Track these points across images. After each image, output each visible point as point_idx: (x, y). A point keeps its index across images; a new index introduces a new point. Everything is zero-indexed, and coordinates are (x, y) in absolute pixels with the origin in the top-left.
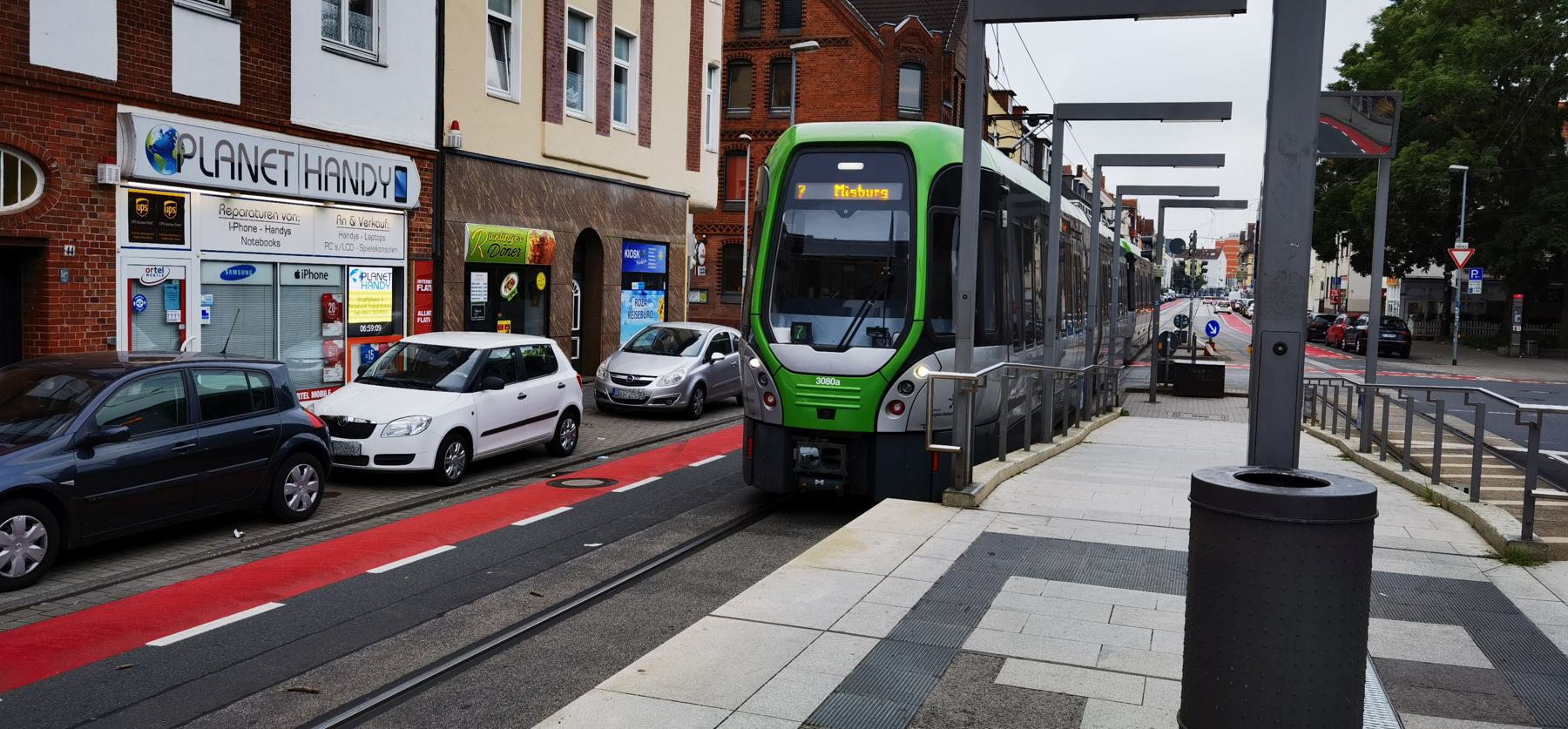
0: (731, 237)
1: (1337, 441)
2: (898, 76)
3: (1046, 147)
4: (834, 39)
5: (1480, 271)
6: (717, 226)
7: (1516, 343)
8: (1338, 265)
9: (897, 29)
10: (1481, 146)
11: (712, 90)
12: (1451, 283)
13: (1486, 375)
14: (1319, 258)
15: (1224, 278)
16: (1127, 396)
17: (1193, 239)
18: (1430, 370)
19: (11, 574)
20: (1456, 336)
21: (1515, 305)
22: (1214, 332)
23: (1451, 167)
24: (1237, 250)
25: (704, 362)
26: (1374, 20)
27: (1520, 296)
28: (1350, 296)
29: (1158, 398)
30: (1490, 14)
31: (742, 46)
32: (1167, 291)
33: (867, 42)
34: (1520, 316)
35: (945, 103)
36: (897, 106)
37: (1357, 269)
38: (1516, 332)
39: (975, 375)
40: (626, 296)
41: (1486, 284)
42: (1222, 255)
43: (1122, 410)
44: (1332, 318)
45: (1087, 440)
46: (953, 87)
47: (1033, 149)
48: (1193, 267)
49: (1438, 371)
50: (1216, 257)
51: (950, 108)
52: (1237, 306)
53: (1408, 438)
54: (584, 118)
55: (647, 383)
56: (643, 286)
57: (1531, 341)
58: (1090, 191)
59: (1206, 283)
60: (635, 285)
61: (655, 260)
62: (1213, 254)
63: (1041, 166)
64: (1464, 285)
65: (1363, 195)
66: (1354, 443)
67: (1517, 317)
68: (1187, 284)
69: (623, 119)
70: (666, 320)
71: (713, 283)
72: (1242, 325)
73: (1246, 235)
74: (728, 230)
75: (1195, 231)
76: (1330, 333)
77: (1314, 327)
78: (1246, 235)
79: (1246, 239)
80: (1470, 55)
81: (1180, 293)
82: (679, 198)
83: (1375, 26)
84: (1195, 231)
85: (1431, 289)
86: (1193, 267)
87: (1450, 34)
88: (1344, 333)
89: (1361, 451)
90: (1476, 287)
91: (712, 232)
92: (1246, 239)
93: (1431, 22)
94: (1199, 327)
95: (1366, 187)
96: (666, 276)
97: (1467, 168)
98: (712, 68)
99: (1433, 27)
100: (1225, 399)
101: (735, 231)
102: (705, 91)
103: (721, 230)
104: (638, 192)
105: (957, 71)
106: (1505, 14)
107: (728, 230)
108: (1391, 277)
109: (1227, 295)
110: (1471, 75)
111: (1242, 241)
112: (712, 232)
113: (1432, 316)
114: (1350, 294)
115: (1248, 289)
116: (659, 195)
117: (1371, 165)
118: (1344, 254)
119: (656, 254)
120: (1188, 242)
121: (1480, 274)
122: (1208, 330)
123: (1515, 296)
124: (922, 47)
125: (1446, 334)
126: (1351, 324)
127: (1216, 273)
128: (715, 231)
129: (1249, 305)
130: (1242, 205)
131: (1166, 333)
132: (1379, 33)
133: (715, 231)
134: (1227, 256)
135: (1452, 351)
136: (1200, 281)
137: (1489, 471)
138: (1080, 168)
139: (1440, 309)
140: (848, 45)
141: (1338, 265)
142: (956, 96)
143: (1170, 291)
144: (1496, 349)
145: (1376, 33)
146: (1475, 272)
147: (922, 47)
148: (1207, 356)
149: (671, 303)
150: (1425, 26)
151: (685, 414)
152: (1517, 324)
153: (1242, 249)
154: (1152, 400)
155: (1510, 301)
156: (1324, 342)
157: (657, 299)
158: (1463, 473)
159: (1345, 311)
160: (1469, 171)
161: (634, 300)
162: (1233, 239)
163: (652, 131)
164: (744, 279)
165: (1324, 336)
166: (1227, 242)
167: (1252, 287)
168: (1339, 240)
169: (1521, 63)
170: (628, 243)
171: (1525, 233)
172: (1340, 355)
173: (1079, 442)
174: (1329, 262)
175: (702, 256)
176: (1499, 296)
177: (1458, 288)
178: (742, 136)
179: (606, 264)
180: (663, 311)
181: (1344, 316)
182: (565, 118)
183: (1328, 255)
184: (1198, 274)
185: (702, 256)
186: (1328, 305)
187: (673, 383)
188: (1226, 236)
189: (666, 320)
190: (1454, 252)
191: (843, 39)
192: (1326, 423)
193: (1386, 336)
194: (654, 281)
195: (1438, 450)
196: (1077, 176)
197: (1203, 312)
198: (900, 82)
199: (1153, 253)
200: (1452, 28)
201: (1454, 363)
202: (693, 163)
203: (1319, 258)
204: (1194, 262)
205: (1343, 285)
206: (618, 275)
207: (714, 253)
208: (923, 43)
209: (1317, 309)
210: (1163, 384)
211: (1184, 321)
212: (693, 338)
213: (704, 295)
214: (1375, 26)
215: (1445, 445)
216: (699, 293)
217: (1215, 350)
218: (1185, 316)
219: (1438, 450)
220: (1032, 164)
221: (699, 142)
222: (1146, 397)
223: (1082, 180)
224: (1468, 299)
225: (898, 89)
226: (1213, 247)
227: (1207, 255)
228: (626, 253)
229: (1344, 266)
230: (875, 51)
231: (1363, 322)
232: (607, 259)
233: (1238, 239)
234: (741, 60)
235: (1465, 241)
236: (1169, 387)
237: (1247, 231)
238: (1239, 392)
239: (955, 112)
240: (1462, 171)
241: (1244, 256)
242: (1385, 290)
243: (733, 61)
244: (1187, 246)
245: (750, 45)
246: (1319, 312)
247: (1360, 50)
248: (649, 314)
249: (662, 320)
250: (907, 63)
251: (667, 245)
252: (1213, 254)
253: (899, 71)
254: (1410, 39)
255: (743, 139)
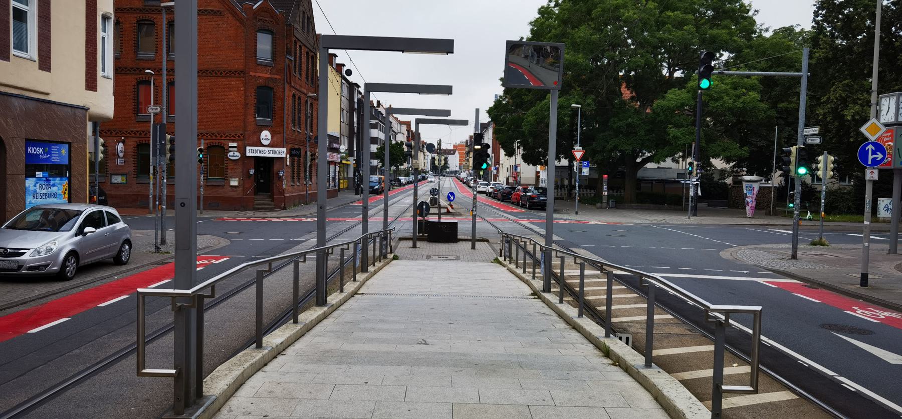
0: (143, 139)
1: (527, 280)
2: (256, 37)
3: (356, 88)
4: (212, 11)
5: (588, 163)
6: (132, 132)
7: (605, 201)
8: (516, 159)
9: (254, 7)
10: (586, 95)
11: (107, 35)
12: (574, 169)
13: (596, 219)
14: (506, 155)
15: (458, 165)
16: (399, 242)
17: (439, 144)
18: (565, 218)
19: (67, 262)
20: (577, 198)
21: (604, 180)
22: (452, 198)
23: (573, 105)
24: (464, 150)
25: (76, 235)
26: (531, 23)
27: (606, 176)
28: (522, 176)
29: (419, 244)
30: (588, 24)
31: (147, 11)
32: (428, 173)
33: (234, 14)
34: (606, 187)
35: (288, 57)
36: (256, 57)
37: (525, 161)
38: (605, 195)
39: (190, 291)
40: (30, 183)
41: (590, 169)
42: (457, 152)
43: (394, 256)
44: (514, 189)
45: (360, 292)
46: (293, 47)
47: (348, 89)
48: (440, 161)
49: (569, 218)
50: (454, 154)
51: (291, 60)
52: (465, 181)
53: (562, 268)
54: (29, 57)
55: (23, 254)
56: (47, 175)
57: (612, 200)
58: (384, 115)
59: (449, 168)
60: (39, 174)
61: (60, 155)
62: (452, 152)
63: (354, 100)
64: (580, 170)
65: (528, 120)
66: (539, 284)
67: (605, 187)
68: (439, 170)
69: (25, 49)
70: (70, 201)
71: (131, 169)
72: (468, 192)
73: (469, 142)
74: (140, 134)
75: (440, 139)
76: (513, 196)
77: (504, 193)
78: (469, 142)
79: (469, 144)
80: (579, 45)
81: (436, 173)
82: (80, 110)
83: (531, 27)
84: (440, 139)
85: (562, 172)
86: (440, 161)
87: (569, 33)
88: (521, 197)
89: (544, 291)
90: (586, 171)
91: (128, 135)
92: (469, 144)
93: (559, 26)
94: (445, 193)
95: (529, 116)
96: (69, 167)
97: (580, 106)
98: (105, 18)
99: (561, 28)
100: (458, 243)
101: (145, 134)
102: (100, 34)
103: (239, 137)
104: (39, 104)
105: (296, 37)
106: (595, 24)
107: (140, 134)
108: (542, 165)
109: (460, 174)
110: (580, 56)
111: (467, 145)
112: (128, 135)
113: (563, 186)
114: (522, 174)
115: (470, 171)
116: (61, 108)
117: (543, 94)
118: (518, 153)
119: (59, 150)
120: (436, 145)
121: (588, 164)
122: (449, 197)
123: (604, 176)
124: (272, 20)
125: (571, 197)
126: (524, 192)
127: (454, 162)
128: (211, 137)
129: (471, 180)
130: (465, 123)
131: (422, 203)
132: (534, 31)
133: (235, 137)
134: (459, 153)
135: (575, 208)
136: (446, 166)
137: (621, 302)
138: (378, 102)
139: (566, 182)
140: (222, 15)
141: (516, 159)
142: (296, 53)
143: (430, 172)
144: (595, 204)
145: (532, 31)
146: (585, 163)
147: (272, 20)
148: (448, 213)
149: (73, 186)
150: (556, 29)
151: (60, 276)
152: (605, 191)
153: (467, 149)
154: (414, 246)
155: (601, 178)
156: (510, 202)
157: (61, 184)
158: (600, 295)
159: (520, 185)
160: (581, 108)
161: (38, 185)
162: (462, 144)
163: (51, 59)
164: (151, 168)
165: (510, 199)
166: (459, 145)
167: (472, 170)
168: (516, 145)
169: (604, 51)
170: (30, 142)
171: (608, 142)
172: (519, 210)
173: (355, 293)
174: (511, 157)
175: (122, 152)
176: (596, 176)
177: (577, 172)
178: (146, 71)
179: (9, 158)
180: (67, 192)
181: (520, 187)
182: (11, 57)
183: (510, 153)
184: (442, 165)
185: (122, 152)
186: (511, 180)
187: (46, 253)
188: (458, 142)
189: (70, 201)
190: (575, 152)
191: (218, 11)
192: (519, 258)
193: (542, 198)
194: (57, 170)
195: (582, 276)
196: (377, 107)
197: (447, 184)
198: (258, 39)
199: (413, 153)
200: (569, 30)
201: (577, 213)
202: (91, 84)
203: (506, 155)
204: (440, 157)
205: (519, 170)
206: (22, 166)
207: (131, 150)
208: (272, 17)
209: (505, 183)
210: (421, 234)
211: (436, 191)
212: (71, 216)
213: (124, 178)
214: (531, 27)
215: (587, 272)
216: (120, 177)
217: (452, 208)
218: (436, 189)
219: (582, 276)
220: (348, 98)
221: (96, 71)
222: (410, 243)
223: (380, 109)
224: (582, 178)
225: (256, 46)
226: (452, 148)
227: (451, 152)
228: (29, 150)
229: (518, 159)
230: (240, 20)
231: (530, 191)
232: (9, 154)
233: (465, 144)
234: (148, 20)
235: (580, 146)
236: (425, 236)
237: (469, 140)
238: (466, 238)
239: (295, 63)
240: (578, 107)
241: (468, 153)
242: (539, 172)
243: (141, 20)
244: (436, 148)
245: (153, 11)
246: (507, 184)
247: (524, 40)
248: (54, 195)
249: (66, 200)
250: (261, 30)
251: (70, 144)
252: (452, 152)
253: (256, 34)
254: (549, 35)
255: (147, 73)
